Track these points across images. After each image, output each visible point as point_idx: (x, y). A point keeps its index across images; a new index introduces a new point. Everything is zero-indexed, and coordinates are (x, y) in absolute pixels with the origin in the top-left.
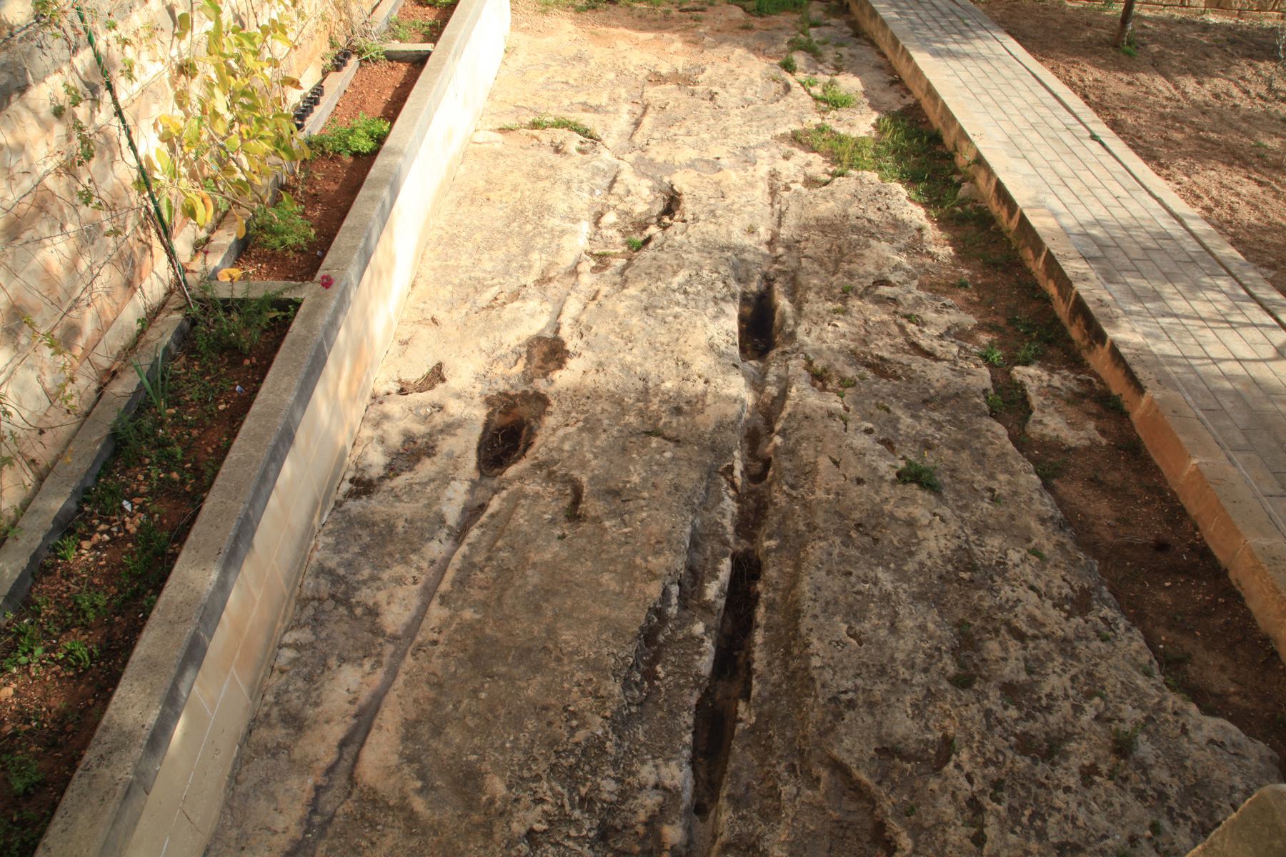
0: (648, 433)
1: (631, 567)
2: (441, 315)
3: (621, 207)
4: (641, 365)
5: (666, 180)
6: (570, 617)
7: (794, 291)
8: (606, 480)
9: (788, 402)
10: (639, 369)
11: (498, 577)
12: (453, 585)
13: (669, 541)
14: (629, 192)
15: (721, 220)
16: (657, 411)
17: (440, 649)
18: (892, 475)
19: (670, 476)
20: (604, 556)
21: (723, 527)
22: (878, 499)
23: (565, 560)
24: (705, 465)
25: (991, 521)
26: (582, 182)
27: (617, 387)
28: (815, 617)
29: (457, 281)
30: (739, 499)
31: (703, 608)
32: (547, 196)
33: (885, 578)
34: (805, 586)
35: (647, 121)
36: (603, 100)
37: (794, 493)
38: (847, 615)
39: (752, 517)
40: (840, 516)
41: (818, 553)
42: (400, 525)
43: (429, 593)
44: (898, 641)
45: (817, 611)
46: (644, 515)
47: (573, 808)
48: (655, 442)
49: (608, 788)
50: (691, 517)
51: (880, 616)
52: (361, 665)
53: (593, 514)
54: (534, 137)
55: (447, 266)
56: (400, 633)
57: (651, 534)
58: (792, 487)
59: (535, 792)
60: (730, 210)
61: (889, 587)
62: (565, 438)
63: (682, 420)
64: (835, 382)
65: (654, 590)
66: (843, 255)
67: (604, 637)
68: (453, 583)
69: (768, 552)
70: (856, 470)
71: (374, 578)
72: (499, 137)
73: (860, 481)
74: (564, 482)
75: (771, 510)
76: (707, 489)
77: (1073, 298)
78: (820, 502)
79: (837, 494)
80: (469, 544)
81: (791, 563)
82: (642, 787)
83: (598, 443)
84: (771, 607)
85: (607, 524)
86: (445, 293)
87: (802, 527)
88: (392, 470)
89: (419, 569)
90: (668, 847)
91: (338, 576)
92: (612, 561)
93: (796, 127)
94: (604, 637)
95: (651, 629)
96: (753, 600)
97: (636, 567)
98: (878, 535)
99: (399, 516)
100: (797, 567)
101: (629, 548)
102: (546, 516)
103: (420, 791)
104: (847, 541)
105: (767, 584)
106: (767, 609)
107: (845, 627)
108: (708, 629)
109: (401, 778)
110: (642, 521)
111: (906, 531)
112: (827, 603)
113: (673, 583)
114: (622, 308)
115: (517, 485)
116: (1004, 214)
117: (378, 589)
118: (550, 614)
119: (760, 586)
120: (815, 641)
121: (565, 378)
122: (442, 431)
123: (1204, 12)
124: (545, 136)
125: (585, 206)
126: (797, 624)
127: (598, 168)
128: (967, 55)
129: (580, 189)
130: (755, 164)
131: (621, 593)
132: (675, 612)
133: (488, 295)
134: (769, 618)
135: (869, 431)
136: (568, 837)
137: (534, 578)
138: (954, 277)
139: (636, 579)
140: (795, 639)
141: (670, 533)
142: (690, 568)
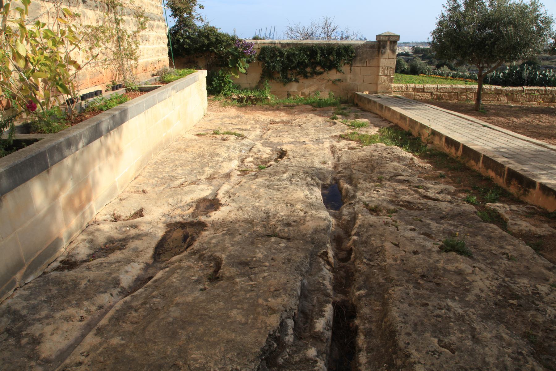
1: (254, 305)
2: (147, 189)
3: (255, 156)
5: (279, 147)
6: (200, 340)
7: (350, 180)
8: (239, 257)
9: (357, 221)
10: (263, 208)
11: (148, 314)
12: (109, 322)
13: (284, 289)
14: (259, 151)
16: (275, 225)
18: (436, 248)
20: (234, 299)
21: (324, 285)
23: (202, 302)
24: (308, 250)
25: (514, 270)
27: (249, 216)
28: (409, 334)
29: (161, 176)
30: (333, 270)
31: (314, 338)
32: (217, 150)
33: (456, 307)
34: (395, 313)
36: (249, 127)
37: (372, 263)
38: (434, 332)
39: (344, 282)
40: (408, 272)
41: (399, 293)
42: (83, 283)
43: (89, 327)
44: (483, 348)
45: (409, 330)
46: (266, 274)
48: (273, 239)
50: (300, 278)
51: (462, 332)
53: (228, 275)
54: (214, 137)
55: (157, 171)
56: (53, 357)
57: (271, 285)
58: (369, 260)
61: (460, 311)
63: (291, 228)
64: (384, 212)
65: (274, 321)
67: (229, 356)
68: (110, 320)
69: (360, 298)
70: (411, 247)
71: (47, 317)
72: (197, 137)
73: (415, 253)
74: (210, 261)
75: (357, 274)
76: (311, 264)
77: (506, 172)
78: (391, 265)
79: (402, 260)
81: (379, 303)
83: (235, 239)
84: (368, 334)
85: (238, 280)
86: (153, 181)
87: (381, 280)
88: (93, 256)
91: (20, 315)
92: (240, 302)
93: (341, 133)
94: (229, 356)
95: (271, 353)
96: (355, 332)
97: (259, 305)
98: (439, 281)
100: (385, 304)
101: (254, 293)
102: (193, 278)
104: (417, 285)
105: (363, 318)
106: (366, 336)
107: (436, 340)
108: (319, 353)
110: (264, 278)
111: (458, 278)
112: (416, 324)
113: (288, 317)
115: (177, 264)
116: (453, 150)
118: (184, 337)
119: (357, 322)
120: (413, 351)
121: (216, 216)
122: (133, 238)
123: (507, 103)
126: (394, 341)
128: (415, 109)
129: (234, 149)
130: (323, 143)
131: (246, 323)
132: (291, 340)
133: (178, 182)
134: (368, 342)
137: (175, 313)
138: (435, 175)
139: (259, 313)
140: (395, 352)
141: (285, 284)
142: (302, 311)
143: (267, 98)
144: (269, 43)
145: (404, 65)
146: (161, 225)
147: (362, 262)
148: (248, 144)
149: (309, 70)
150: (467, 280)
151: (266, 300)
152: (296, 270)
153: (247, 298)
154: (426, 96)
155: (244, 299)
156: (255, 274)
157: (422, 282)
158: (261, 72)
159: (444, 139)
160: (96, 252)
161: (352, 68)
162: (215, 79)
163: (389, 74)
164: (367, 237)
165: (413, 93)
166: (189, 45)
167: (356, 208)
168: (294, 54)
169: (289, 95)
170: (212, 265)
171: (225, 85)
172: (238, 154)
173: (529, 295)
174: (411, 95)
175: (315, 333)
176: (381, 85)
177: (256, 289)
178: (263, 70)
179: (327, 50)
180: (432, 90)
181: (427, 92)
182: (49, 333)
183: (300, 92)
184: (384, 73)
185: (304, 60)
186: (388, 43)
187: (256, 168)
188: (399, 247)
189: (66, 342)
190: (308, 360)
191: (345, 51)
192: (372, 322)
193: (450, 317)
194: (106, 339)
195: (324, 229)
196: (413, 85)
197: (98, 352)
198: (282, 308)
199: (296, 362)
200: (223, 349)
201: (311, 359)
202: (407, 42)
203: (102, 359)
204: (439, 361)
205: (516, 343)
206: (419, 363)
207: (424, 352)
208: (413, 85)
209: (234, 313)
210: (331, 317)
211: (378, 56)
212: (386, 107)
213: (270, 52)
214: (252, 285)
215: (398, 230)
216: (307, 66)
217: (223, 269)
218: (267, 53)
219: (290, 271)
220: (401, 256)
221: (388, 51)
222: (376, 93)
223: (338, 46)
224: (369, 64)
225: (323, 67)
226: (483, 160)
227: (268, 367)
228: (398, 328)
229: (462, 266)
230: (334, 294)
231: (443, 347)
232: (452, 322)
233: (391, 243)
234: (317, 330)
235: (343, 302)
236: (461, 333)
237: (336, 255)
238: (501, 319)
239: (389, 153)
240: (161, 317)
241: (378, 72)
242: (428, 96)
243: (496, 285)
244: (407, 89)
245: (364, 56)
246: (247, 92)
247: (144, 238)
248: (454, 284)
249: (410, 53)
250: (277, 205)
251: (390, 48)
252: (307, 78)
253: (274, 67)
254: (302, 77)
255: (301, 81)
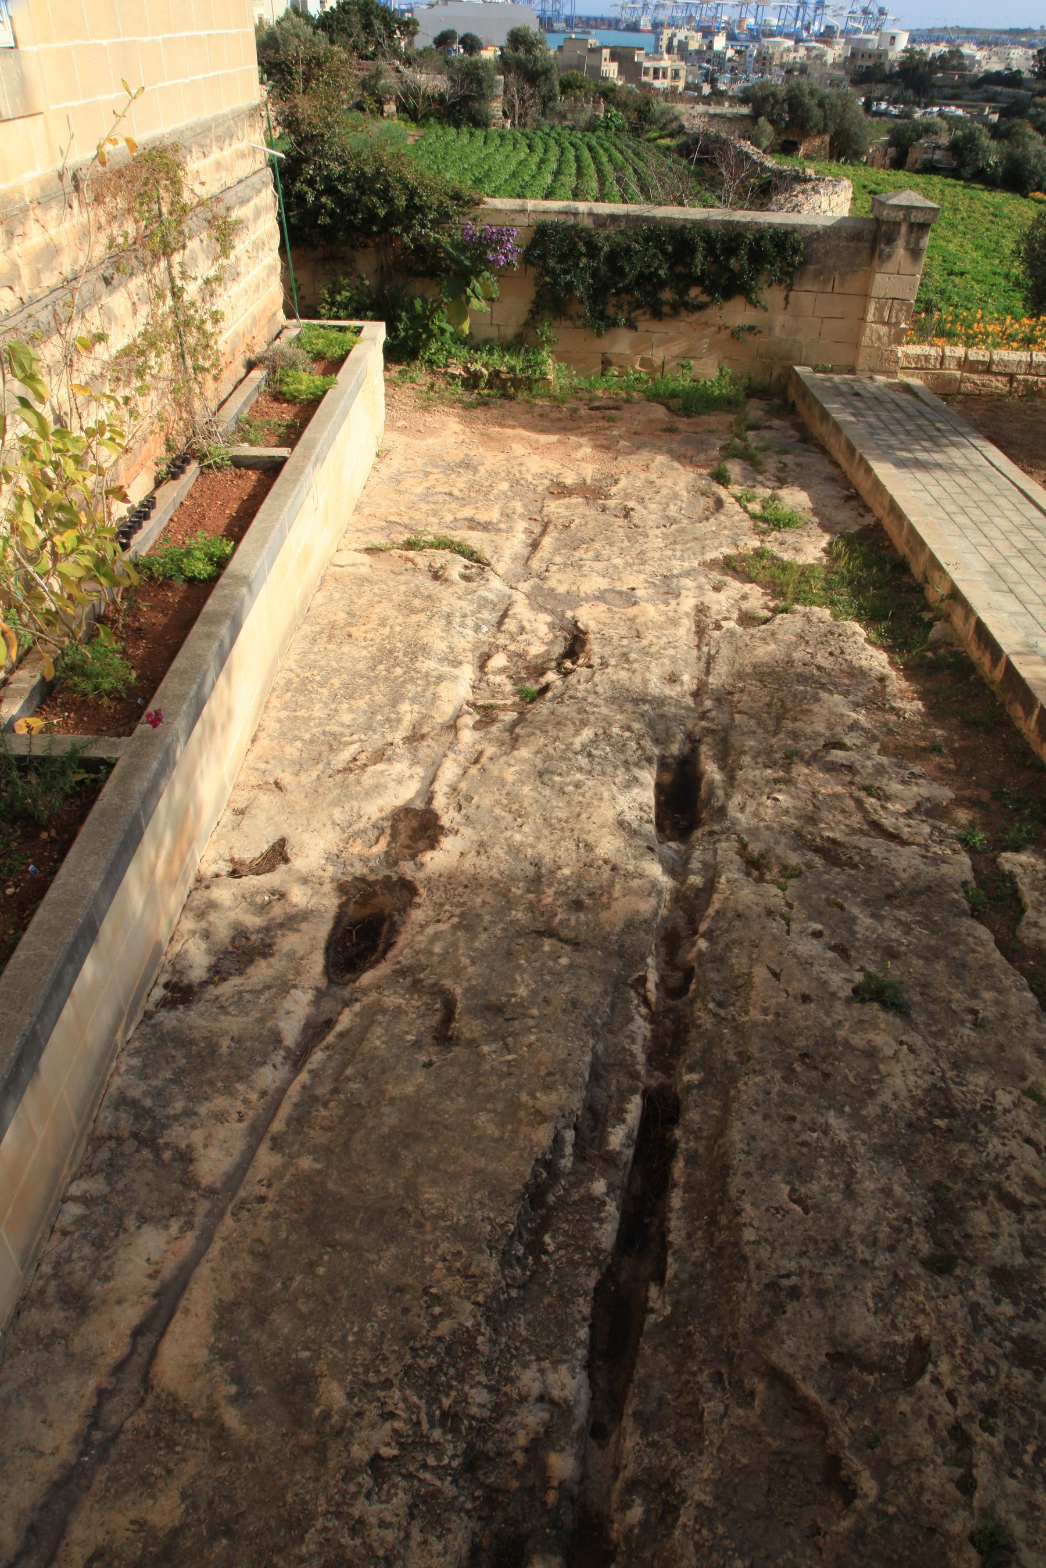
0: (540, 934)
1: (514, 1105)
4: (532, 846)
5: (569, 614)
7: (725, 756)
8: (485, 993)
10: (530, 852)
11: (346, 1115)
13: (563, 1073)
14: (522, 630)
15: (636, 666)
16: (552, 905)
17: (268, 1207)
19: (567, 989)
20: (480, 1090)
21: (632, 1055)
22: (829, 1023)
23: (430, 1095)
25: (973, 1052)
26: (465, 616)
28: (748, 1175)
29: (307, 736)
30: (652, 1019)
31: (605, 1160)
32: (422, 633)
34: (736, 1134)
35: (547, 542)
37: (722, 1013)
38: (789, 1173)
41: (752, 1091)
42: (225, 1043)
43: (257, 1133)
44: (855, 1208)
45: (751, 1167)
46: (533, 1038)
47: (432, 1426)
48: (547, 945)
49: (478, 1400)
50: (591, 1042)
51: (832, 1176)
52: (167, 1227)
53: (468, 1035)
56: (218, 1185)
57: (540, 1063)
58: (720, 1004)
59: (384, 1404)
60: (647, 654)
61: (844, 1137)
62: (436, 937)
63: (582, 917)
65: (543, 1136)
66: (786, 711)
67: (478, 1196)
69: (689, 1087)
70: (800, 985)
71: (188, 1113)
73: (806, 999)
75: (693, 1033)
78: (755, 1025)
79: (777, 1015)
80: (310, 1071)
81: (718, 1103)
82: (523, 1399)
83: (477, 944)
84: (692, 1160)
85: (486, 1049)
86: (292, 751)
87: (732, 1057)
88: (217, 973)
89: (246, 1101)
90: (555, 1483)
92: (491, 1097)
94: (478, 1196)
95: (538, 1186)
97: (521, 1106)
98: (830, 1069)
99: (223, 1033)
100: (726, 1109)
101: (512, 1080)
102: (409, 1037)
103: (234, 1400)
106: (687, 1162)
108: (611, 1188)
109: (210, 1380)
110: (530, 1046)
111: (866, 1064)
112: (764, 1157)
113: (566, 1127)
114: (510, 775)
115: (373, 996)
116: (986, 660)
117: (194, 1127)
118: (410, 1164)
120: (748, 1207)
122: (282, 925)
124: (421, 559)
125: (468, 646)
127: (485, 599)
128: (939, 466)
131: (501, 1138)
132: (569, 1165)
134: (689, 1175)
135: (817, 935)
136: (425, 1466)
137: (391, 1117)
139: (520, 1121)
140: (722, 1204)
141: (565, 1062)
142: (590, 1108)
143: (543, 377)
144: (560, 213)
145: (987, 150)
146: (328, 887)
147: (706, 1008)
148: (496, 600)
149: (667, 295)
150: (878, 1072)
151: (534, 1097)
152: (585, 1026)
153: (503, 1091)
154: (995, 383)
155: (497, 1091)
156: (514, 1035)
157: (798, 1069)
158: (532, 295)
159: (973, 622)
160: (219, 959)
161: (792, 294)
162: (403, 314)
163: (893, 320)
164: (727, 945)
165: (958, 373)
166: (332, 214)
167: (720, 852)
168: (628, 250)
169: (606, 363)
170: (438, 1006)
171: (429, 338)
172: (470, 639)
173: (974, 1110)
174: (951, 380)
175: (608, 1152)
176: (868, 350)
177: (517, 1072)
178: (538, 292)
179: (723, 242)
180: (1013, 369)
181: (1000, 374)
182: (201, 1145)
183: (639, 357)
184: (881, 316)
185: (657, 269)
186: (904, 229)
187: (514, 695)
188: (778, 979)
189: (229, 1159)
190: (591, 1198)
191: (776, 246)
192: (701, 1138)
193: (823, 1148)
194: (291, 1157)
195: (645, 921)
196: (960, 351)
197: (285, 1181)
198: (557, 1112)
199: (574, 1202)
200: (468, 1186)
201: (597, 1198)
202: (1022, 27)
203: (293, 1193)
204: (780, 1225)
205: (909, 1203)
206: (751, 1225)
207: (763, 1208)
208: (960, 351)
209: (482, 1119)
210: (637, 1123)
211: (870, 265)
212: (861, 458)
213: (561, 240)
214: (509, 1062)
215: (788, 932)
216: (661, 284)
217: (459, 1021)
218: (553, 242)
219: (575, 1029)
220: (778, 1003)
221: (900, 251)
222: (852, 370)
223: (758, 231)
224: (842, 285)
225: (708, 291)
226: (1039, 717)
227: (533, 1209)
228: (735, 1162)
229: (879, 1039)
230: (648, 1071)
231: (795, 1201)
232: (823, 1156)
233: (769, 968)
234: (611, 1147)
235: (662, 1088)
236: (830, 1180)
237: (662, 980)
238: (906, 1157)
239: (831, 654)
240: (370, 1124)
241: (865, 311)
242: (1000, 385)
243: (925, 1086)
244: (941, 364)
245: (830, 262)
246: (490, 352)
247: (304, 926)
248: (852, 1080)
249: (1026, 75)
250: (558, 842)
251: (908, 243)
252: (660, 320)
253: (569, 287)
254: (648, 316)
255: (642, 326)
